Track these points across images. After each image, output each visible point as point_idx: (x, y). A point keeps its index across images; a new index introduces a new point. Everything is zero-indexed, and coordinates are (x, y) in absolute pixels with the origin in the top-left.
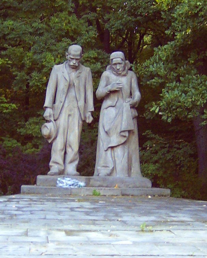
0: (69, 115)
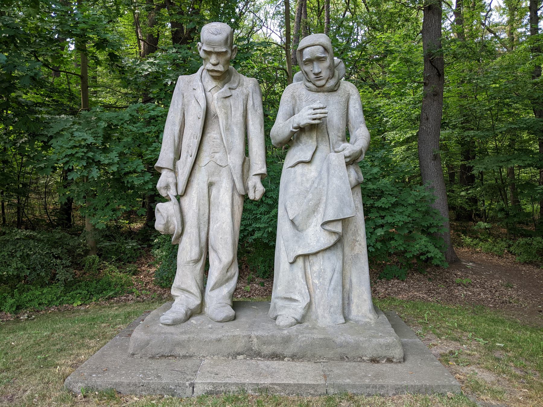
0: (210, 185)
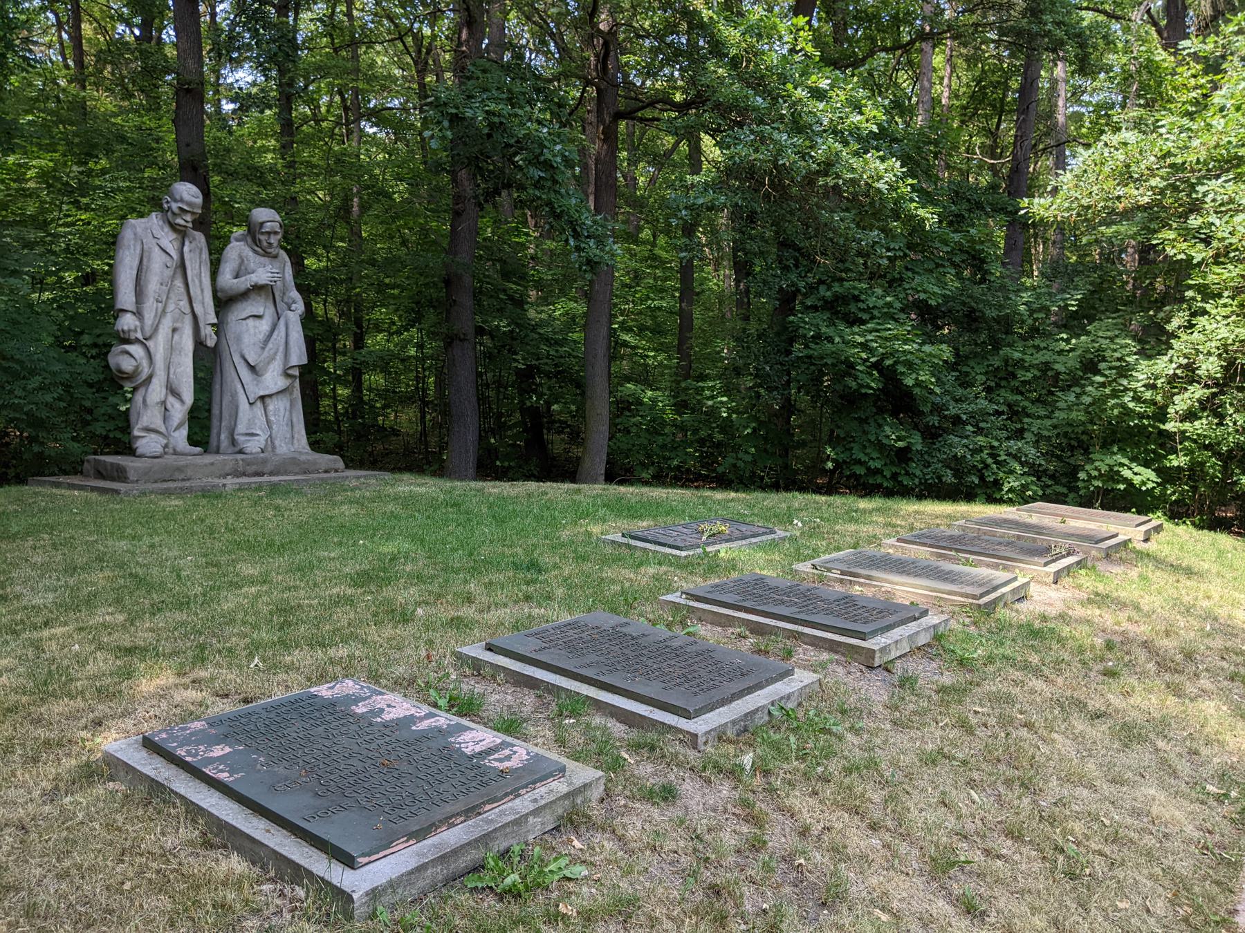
0: (174, 330)
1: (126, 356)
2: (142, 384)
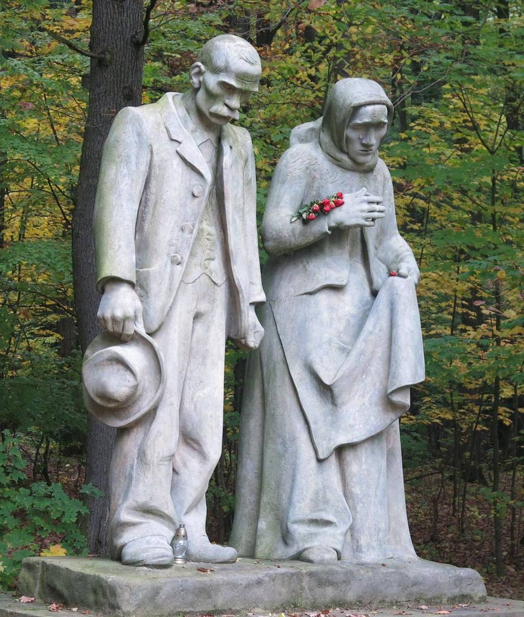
0: (197, 316)
1: (117, 367)
2: (138, 423)
